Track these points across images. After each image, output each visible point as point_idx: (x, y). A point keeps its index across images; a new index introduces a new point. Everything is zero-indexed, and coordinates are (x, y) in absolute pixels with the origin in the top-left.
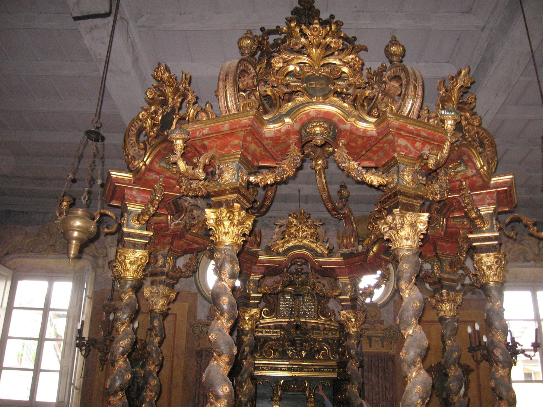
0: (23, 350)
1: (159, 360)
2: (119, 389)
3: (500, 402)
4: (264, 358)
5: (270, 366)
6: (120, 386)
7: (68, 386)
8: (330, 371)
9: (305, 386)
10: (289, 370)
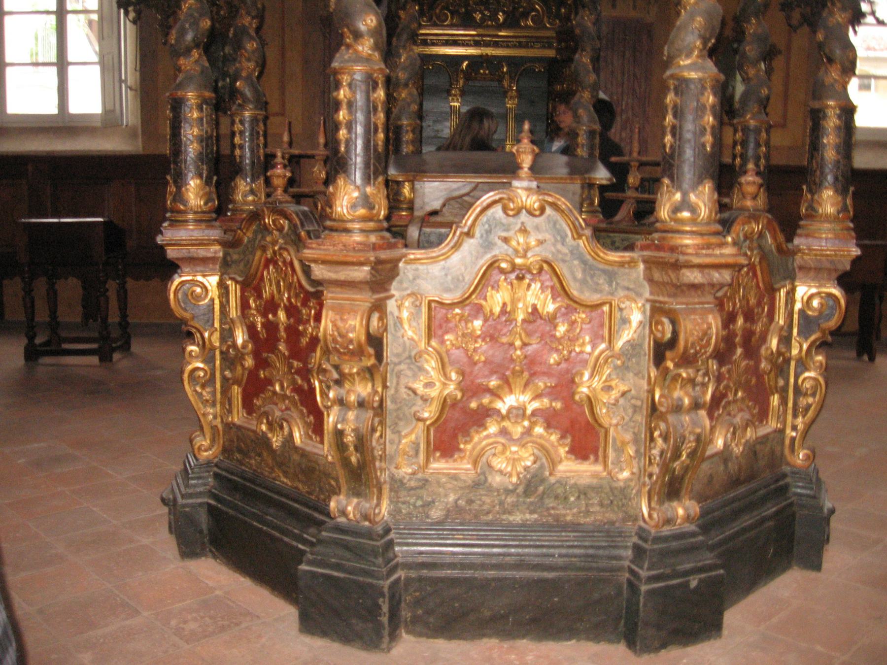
0: (36, 45)
1: (258, 9)
2: (192, 45)
3: (828, 66)
4: (435, 25)
5: (445, 38)
6: (194, 40)
7: (117, 84)
8: (544, 47)
9: (503, 72)
10: (477, 44)
